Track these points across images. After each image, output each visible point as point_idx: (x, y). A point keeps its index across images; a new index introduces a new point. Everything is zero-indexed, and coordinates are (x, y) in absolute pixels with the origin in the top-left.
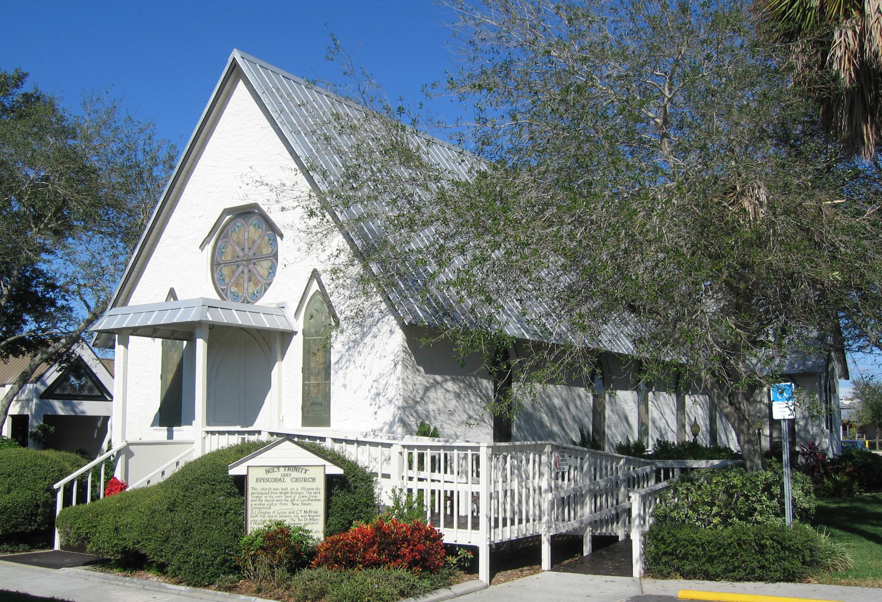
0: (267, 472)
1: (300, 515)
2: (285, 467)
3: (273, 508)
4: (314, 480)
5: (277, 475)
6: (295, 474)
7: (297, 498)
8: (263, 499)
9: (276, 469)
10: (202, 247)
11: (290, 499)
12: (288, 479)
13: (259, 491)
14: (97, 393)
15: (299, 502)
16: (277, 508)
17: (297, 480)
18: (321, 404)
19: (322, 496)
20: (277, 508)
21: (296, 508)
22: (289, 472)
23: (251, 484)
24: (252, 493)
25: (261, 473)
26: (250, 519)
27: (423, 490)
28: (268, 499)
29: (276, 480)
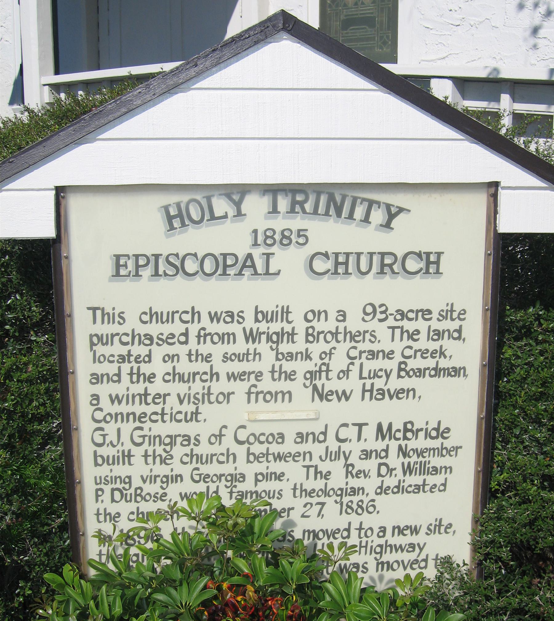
0: (176, 219)
1: (354, 448)
2: (273, 190)
3: (213, 416)
4: (431, 263)
5: (230, 237)
6: (331, 234)
7: (339, 362)
8: (158, 367)
9: (221, 206)
10: (313, 400)
11: (301, 367)
12: (289, 260)
13: (132, 323)
14: (249, 263)
15: (353, 384)
16: (235, 413)
17: (342, 264)
18: (369, 21)
19: (470, 350)
20: (235, 413)
21: (333, 413)
22: (296, 223)
23: (87, 284)
24: (96, 340)
25: (142, 228)
26: (89, 473)
27: (118, 262)
28: (185, 367)
29: (223, 265)
